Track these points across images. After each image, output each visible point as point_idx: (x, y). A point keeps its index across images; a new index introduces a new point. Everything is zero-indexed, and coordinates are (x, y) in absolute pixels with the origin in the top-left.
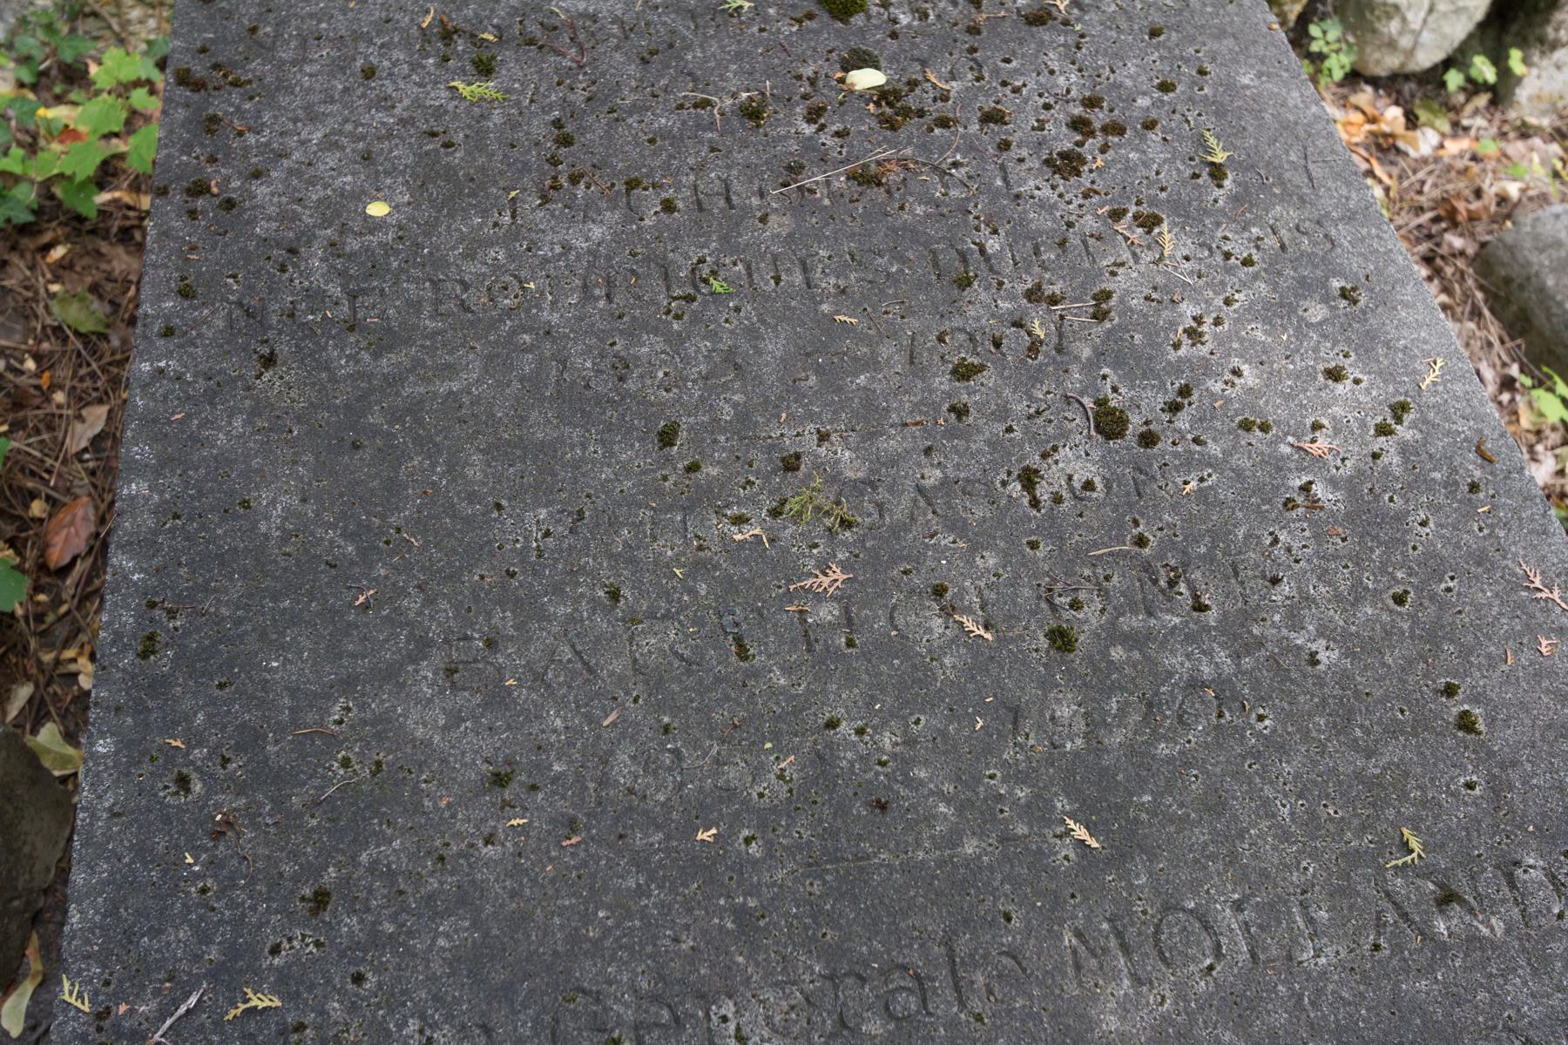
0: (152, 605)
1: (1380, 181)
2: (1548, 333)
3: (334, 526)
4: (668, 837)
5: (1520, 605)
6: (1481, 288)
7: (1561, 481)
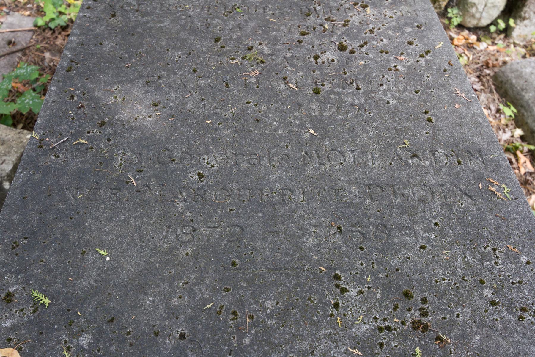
0: (72, 62)
1: (467, 56)
2: (512, 96)
3: (123, 51)
4: (198, 121)
5: (452, 97)
6: (494, 84)
7: (512, 139)
